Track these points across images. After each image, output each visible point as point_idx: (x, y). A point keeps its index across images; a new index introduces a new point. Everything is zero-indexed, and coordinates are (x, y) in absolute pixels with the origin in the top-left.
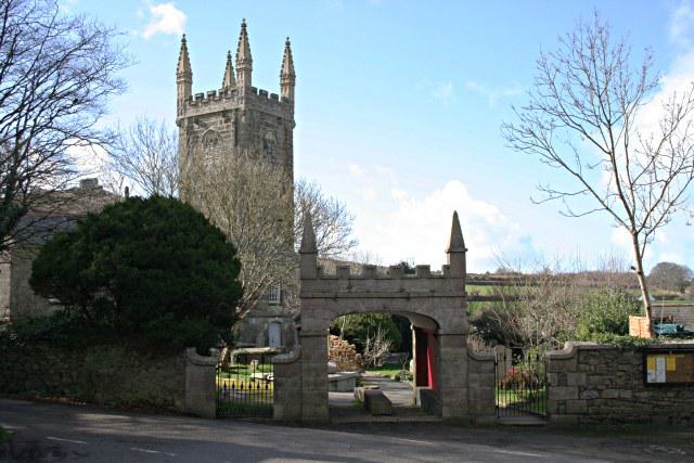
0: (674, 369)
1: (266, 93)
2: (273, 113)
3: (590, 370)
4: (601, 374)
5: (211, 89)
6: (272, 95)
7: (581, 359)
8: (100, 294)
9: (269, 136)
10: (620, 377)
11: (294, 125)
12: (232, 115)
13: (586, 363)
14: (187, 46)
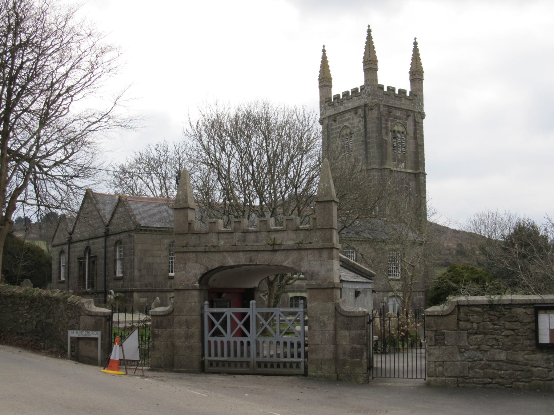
0: (33, 222)
1: (393, 90)
2: (402, 107)
3: (472, 328)
4: (485, 334)
5: (354, 87)
6: (400, 91)
7: (462, 315)
8: (406, 326)
9: (397, 128)
10: (507, 336)
11: (423, 116)
12: (360, 111)
13: (468, 321)
14: (327, 55)
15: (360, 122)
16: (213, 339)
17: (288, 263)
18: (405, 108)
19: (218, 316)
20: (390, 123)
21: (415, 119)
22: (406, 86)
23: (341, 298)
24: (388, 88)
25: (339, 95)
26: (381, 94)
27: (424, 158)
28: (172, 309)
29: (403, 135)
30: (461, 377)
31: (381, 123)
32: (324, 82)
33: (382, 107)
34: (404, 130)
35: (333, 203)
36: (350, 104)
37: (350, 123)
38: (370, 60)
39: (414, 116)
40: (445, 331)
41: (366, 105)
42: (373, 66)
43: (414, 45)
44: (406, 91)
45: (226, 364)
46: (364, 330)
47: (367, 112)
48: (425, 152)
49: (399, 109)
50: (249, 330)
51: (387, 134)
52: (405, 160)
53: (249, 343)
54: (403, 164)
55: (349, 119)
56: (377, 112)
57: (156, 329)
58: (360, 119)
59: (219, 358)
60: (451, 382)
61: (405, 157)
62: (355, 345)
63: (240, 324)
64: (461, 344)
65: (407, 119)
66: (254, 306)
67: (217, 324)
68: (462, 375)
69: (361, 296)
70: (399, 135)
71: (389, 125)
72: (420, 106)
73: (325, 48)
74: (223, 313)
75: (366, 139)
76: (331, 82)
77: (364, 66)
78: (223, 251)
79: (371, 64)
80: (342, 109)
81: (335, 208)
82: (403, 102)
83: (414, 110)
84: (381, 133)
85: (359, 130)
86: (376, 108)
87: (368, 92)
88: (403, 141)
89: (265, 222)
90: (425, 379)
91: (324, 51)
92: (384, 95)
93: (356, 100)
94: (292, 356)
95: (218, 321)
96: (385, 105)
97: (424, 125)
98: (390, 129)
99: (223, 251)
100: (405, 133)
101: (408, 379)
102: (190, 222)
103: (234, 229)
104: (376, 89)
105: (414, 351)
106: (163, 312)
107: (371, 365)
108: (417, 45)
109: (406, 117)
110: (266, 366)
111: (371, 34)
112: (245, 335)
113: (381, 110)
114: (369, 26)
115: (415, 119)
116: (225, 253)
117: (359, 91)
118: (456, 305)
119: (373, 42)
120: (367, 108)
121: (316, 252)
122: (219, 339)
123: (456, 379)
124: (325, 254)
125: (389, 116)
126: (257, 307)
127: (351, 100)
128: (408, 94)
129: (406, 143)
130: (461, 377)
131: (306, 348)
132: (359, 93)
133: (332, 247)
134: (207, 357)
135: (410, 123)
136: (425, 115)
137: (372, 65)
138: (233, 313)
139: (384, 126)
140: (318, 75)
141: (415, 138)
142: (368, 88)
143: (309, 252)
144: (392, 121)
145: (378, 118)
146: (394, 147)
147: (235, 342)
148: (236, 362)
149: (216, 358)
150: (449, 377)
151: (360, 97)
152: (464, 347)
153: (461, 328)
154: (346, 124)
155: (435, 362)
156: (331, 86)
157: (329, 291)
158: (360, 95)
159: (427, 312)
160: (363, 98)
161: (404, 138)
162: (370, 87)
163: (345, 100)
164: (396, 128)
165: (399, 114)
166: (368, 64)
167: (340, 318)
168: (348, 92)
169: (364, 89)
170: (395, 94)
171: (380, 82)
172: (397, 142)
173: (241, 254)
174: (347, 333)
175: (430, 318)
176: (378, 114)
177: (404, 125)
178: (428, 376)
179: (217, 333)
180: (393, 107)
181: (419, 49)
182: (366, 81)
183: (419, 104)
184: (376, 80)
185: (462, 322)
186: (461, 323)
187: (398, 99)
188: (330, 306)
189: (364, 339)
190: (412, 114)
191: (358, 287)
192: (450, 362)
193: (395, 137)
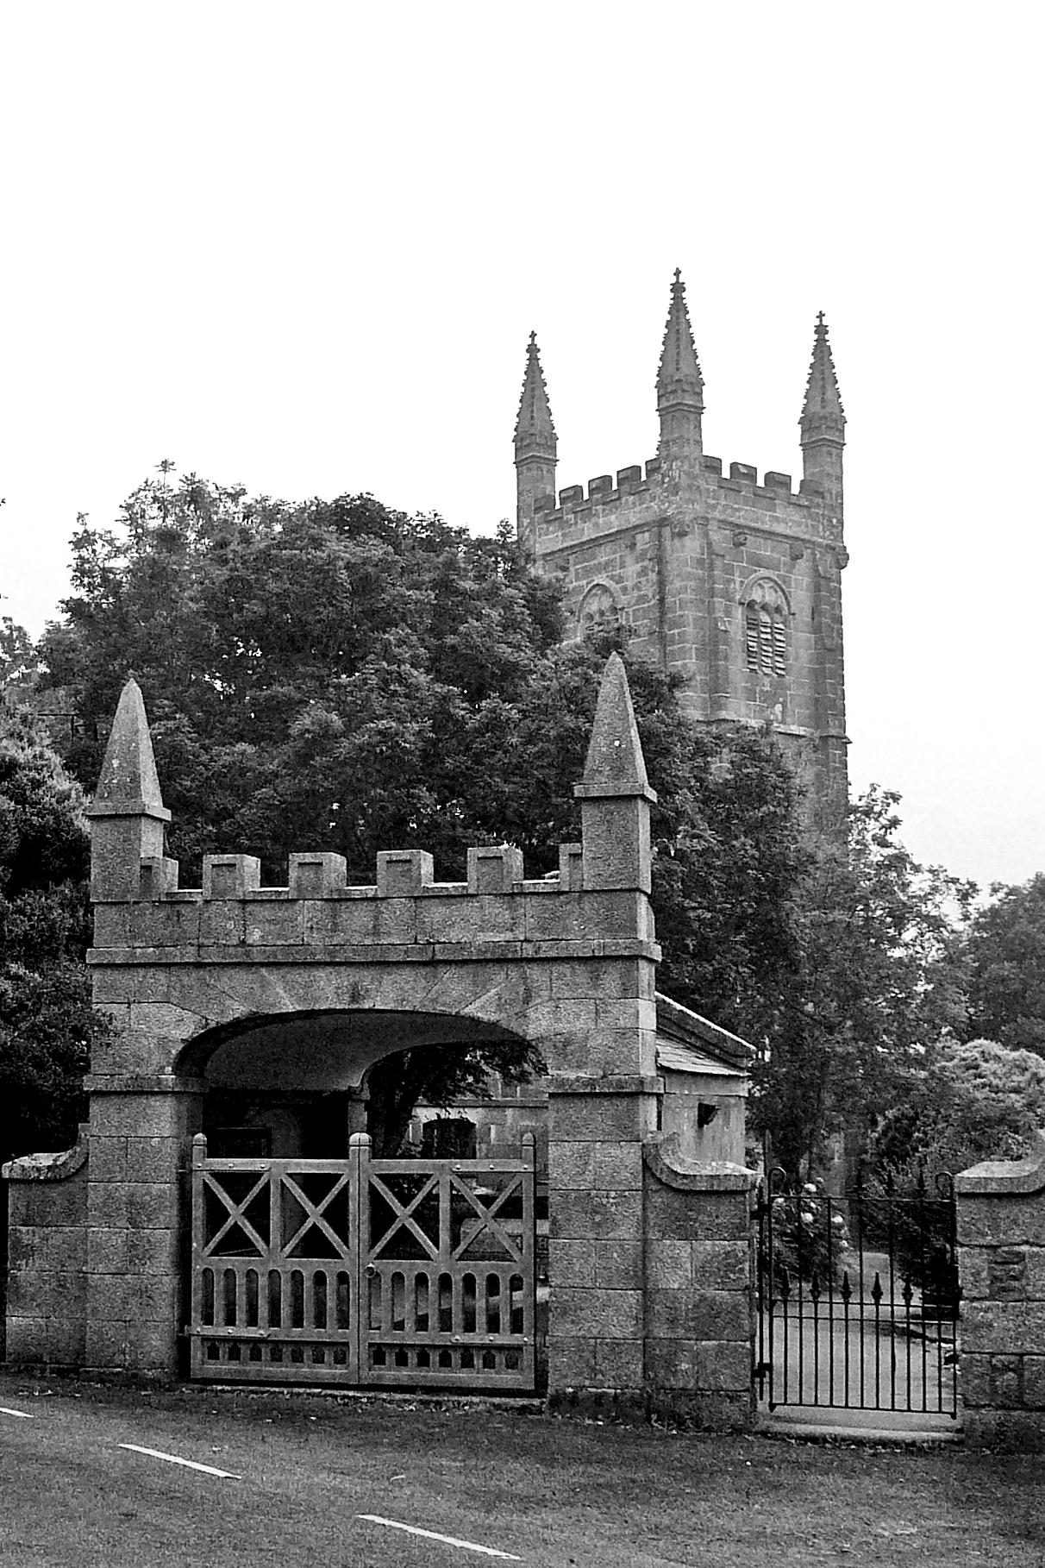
1: (752, 473)
2: (779, 528)
6: (770, 477)
11: (841, 559)
15: (643, 572)
17: (483, 1007)
18: (788, 532)
19: (237, 1184)
22: (793, 466)
23: (659, 1128)
24: (734, 466)
25: (577, 489)
26: (712, 488)
29: (777, 617)
33: (713, 526)
34: (781, 601)
35: (640, 803)
36: (613, 518)
37: (612, 578)
38: (679, 381)
45: (265, 1352)
46: (742, 1239)
47: (668, 543)
50: (343, 1233)
53: (343, 1278)
54: (779, 707)
55: (607, 564)
57: (24, 1229)
59: (241, 1331)
62: (710, 1292)
63: (315, 1215)
67: (236, 1213)
69: (718, 1121)
70: (765, 618)
74: (257, 1176)
75: (661, 627)
78: (262, 965)
79: (684, 391)
80: (588, 532)
81: (643, 819)
83: (814, 539)
84: (710, 609)
85: (642, 599)
90: (953, 1416)
94: (422, 1323)
95: (316, 1203)
99: (262, 965)
101: (831, 1409)
102: (148, 863)
105: (793, 1311)
107: (766, 1360)
109: (787, 559)
110: (423, 1361)
112: (331, 1253)
114: (678, 273)
116: (263, 971)
120: (667, 531)
121: (580, 969)
124: (611, 979)
128: (795, 489)
131: (491, 1299)
134: (198, 1328)
137: (686, 395)
138: (380, 1176)
142: (671, 469)
143: (558, 969)
145: (700, 562)
146: (750, 653)
147: (297, 1277)
154: (600, 579)
157: (623, 1104)
161: (781, 626)
164: (756, 595)
165: (766, 551)
167: (657, 1200)
171: (708, 450)
172: (759, 637)
174: (683, 1249)
175: (972, 1205)
177: (780, 587)
178: (967, 1405)
179: (236, 1243)
180: (749, 528)
182: (664, 444)
184: (699, 443)
188: (630, 1156)
189: (742, 1270)
190: (808, 552)
191: (711, 1094)
193: (753, 624)
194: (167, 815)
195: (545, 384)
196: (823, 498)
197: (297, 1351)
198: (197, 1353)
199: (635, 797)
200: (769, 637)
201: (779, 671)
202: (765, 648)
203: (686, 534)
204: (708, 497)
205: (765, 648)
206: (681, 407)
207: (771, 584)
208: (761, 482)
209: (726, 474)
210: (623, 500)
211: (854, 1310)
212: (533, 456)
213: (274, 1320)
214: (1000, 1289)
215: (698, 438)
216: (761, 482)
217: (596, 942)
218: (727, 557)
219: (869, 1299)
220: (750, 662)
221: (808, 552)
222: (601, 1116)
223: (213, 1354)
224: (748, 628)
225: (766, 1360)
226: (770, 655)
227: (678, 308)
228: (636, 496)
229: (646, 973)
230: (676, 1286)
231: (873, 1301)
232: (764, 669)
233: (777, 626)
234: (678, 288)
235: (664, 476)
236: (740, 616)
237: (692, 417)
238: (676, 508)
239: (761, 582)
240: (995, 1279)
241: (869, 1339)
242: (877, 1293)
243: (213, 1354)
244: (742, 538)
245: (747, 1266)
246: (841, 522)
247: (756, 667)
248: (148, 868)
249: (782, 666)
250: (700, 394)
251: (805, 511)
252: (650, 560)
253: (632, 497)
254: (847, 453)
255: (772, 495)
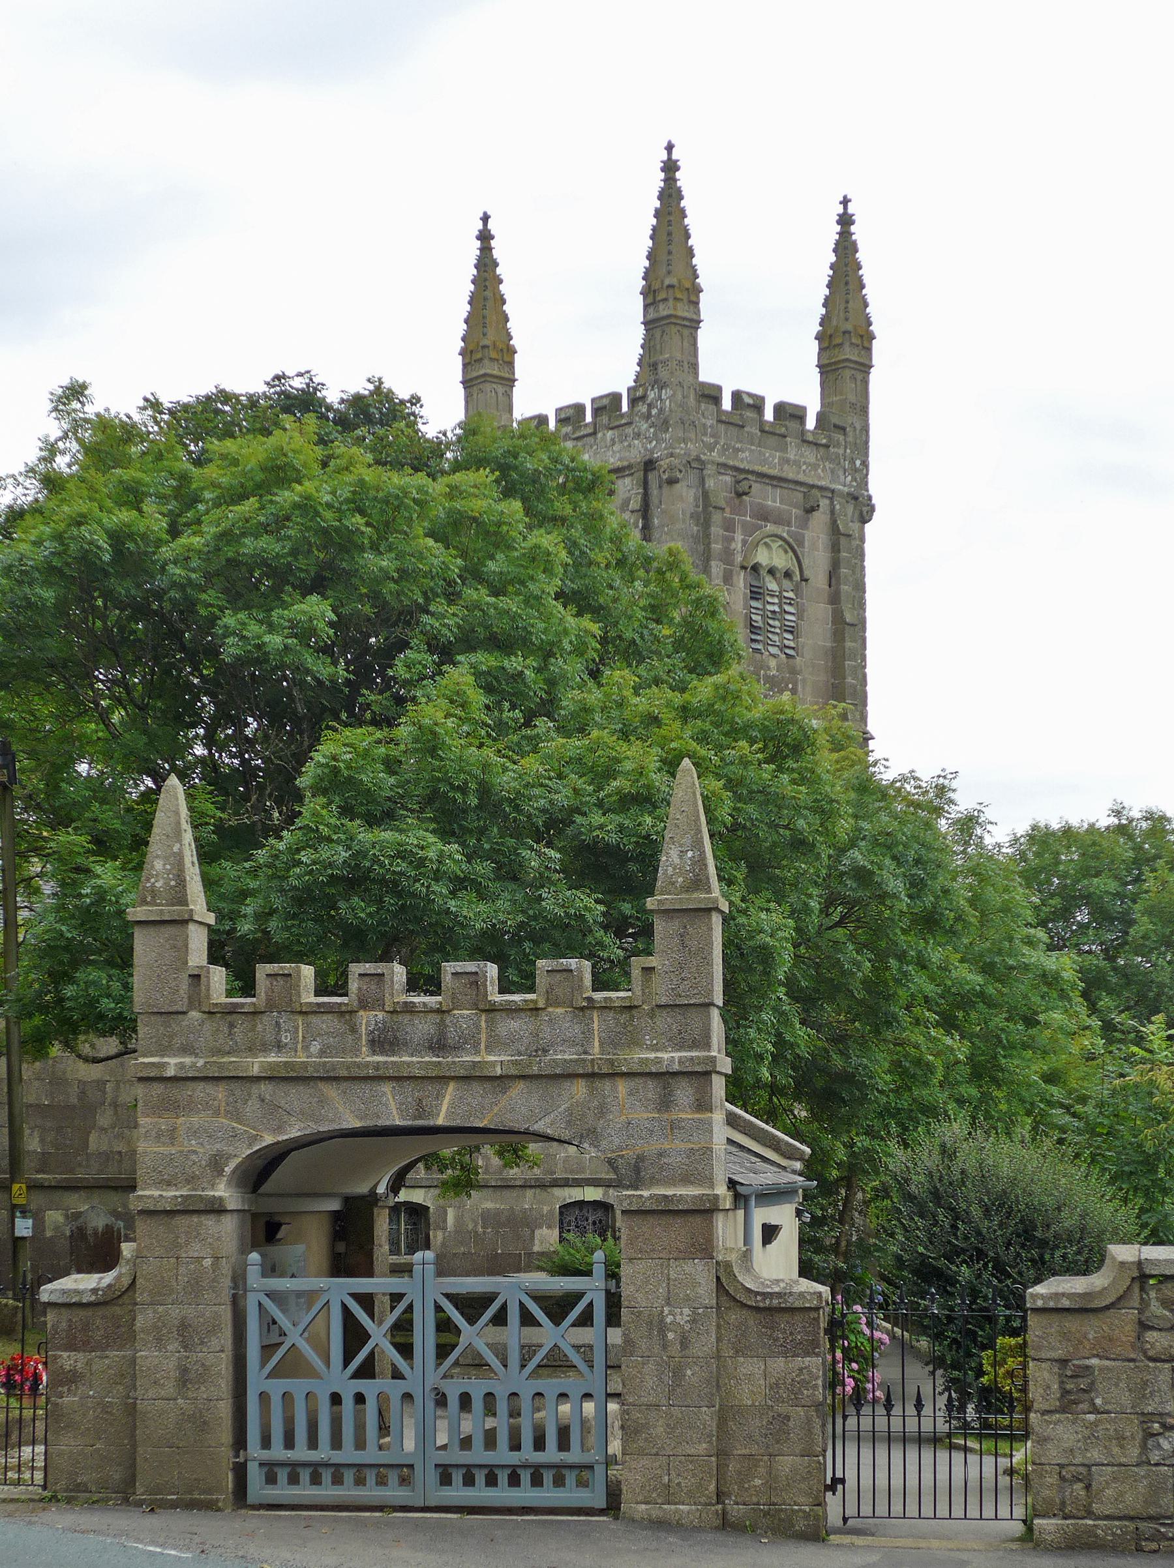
1: (757, 404)
6: (780, 408)
9: (771, 556)
11: (864, 510)
14: (496, 254)
16: (276, 1388)
20: (739, 537)
21: (834, 522)
24: (737, 396)
26: (709, 423)
27: (865, 676)
28: (126, 1282)
29: (786, 583)
30: (1150, 1518)
31: (707, 535)
32: (486, 361)
33: (710, 470)
38: (671, 286)
39: (832, 512)
40: (1094, 1361)
41: (649, 465)
42: (683, 311)
43: (838, 228)
44: (804, 409)
48: (869, 653)
49: (777, 481)
51: (728, 578)
52: (795, 684)
56: (692, 492)
57: (65, 1354)
58: (627, 516)
60: (1113, 1534)
61: (794, 671)
64: (1150, 1409)
65: (804, 524)
66: (430, 1268)
68: (1152, 1511)
70: (773, 586)
71: (737, 545)
72: (856, 470)
73: (491, 225)
76: (511, 364)
77: (646, 307)
79: (675, 299)
82: (791, 455)
83: (833, 486)
86: (693, 477)
87: (661, 411)
88: (788, 608)
89: (472, 979)
91: (485, 237)
92: (722, 427)
93: (613, 442)
96: (725, 465)
97: (868, 547)
98: (739, 559)
100: (797, 577)
103: (360, 1001)
104: (692, 401)
106: (94, 1291)
107: (839, 1475)
108: (853, 228)
109: (800, 512)
110: (514, 1481)
111: (675, 180)
113: (710, 483)
115: (834, 522)
116: (321, 1085)
117: (625, 408)
118: (1136, 1274)
119: (683, 214)
122: (298, 1387)
123: (1131, 1526)
125: (738, 510)
126: (440, 1273)
127: (591, 440)
128: (811, 423)
129: (800, 615)
130: (1150, 1518)
132: (622, 416)
133: (709, 1068)
135: (816, 534)
136: (872, 509)
137: (679, 305)
139: (716, 547)
140: (461, 333)
141: (834, 599)
144: (749, 530)
148: (338, 1466)
149: (289, 1454)
150: (1108, 1518)
151: (629, 430)
152: (1157, 1418)
153: (1150, 1353)
155: (1061, 1466)
156: (510, 382)
157: (698, 1219)
158: (629, 424)
159: (1035, 1296)
160: (637, 435)
161: (791, 595)
162: (669, 392)
163: (566, 437)
164: (762, 557)
165: (773, 500)
166: (665, 300)
167: (734, 1316)
168: (579, 409)
169: (643, 398)
170: (762, 422)
171: (704, 377)
172: (764, 610)
173: (387, 1088)
176: (696, 499)
177: (792, 547)
179: (292, 1366)
180: (752, 472)
181: (860, 245)
183: (853, 462)
184: (694, 367)
185: (1155, 1334)
186: (1151, 1336)
187: (772, 440)
190: (825, 503)
192: (1109, 1468)
194: (211, 919)
195: (501, 282)
196: (845, 434)
197: (294, 1472)
198: (254, 1474)
199: (709, 910)
200: (777, 609)
201: (788, 651)
202: (771, 622)
203: (676, 481)
204: (705, 434)
205: (771, 622)
206: (673, 320)
207: (781, 543)
208: (769, 415)
209: (727, 404)
210: (600, 435)
211: (866, 1423)
212: (485, 375)
213: (336, 1443)
214: (1067, 1404)
215: (692, 360)
216: (769, 415)
217: (671, 1057)
218: (728, 510)
219: (911, 1410)
220: (753, 640)
221: (825, 503)
222: (677, 1233)
223: (271, 1479)
224: (752, 598)
225: (839, 1475)
226: (778, 631)
227: (670, 195)
228: (616, 432)
229: (718, 1087)
230: (749, 1403)
231: (916, 1413)
232: (770, 648)
233: (786, 594)
234: (670, 168)
235: (650, 406)
236: (742, 584)
237: (686, 332)
238: (665, 449)
239: (767, 540)
240: (1065, 1392)
241: (912, 1454)
242: (919, 1405)
243: (271, 1479)
244: (744, 486)
245: (820, 1382)
246: (865, 464)
247: (759, 646)
248: (196, 977)
249: (792, 644)
250: (697, 303)
251: (822, 450)
252: (632, 512)
253: (610, 432)
254: (874, 376)
255: (783, 430)
